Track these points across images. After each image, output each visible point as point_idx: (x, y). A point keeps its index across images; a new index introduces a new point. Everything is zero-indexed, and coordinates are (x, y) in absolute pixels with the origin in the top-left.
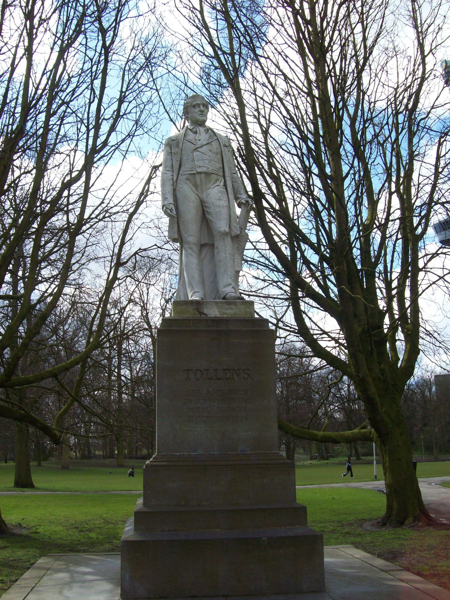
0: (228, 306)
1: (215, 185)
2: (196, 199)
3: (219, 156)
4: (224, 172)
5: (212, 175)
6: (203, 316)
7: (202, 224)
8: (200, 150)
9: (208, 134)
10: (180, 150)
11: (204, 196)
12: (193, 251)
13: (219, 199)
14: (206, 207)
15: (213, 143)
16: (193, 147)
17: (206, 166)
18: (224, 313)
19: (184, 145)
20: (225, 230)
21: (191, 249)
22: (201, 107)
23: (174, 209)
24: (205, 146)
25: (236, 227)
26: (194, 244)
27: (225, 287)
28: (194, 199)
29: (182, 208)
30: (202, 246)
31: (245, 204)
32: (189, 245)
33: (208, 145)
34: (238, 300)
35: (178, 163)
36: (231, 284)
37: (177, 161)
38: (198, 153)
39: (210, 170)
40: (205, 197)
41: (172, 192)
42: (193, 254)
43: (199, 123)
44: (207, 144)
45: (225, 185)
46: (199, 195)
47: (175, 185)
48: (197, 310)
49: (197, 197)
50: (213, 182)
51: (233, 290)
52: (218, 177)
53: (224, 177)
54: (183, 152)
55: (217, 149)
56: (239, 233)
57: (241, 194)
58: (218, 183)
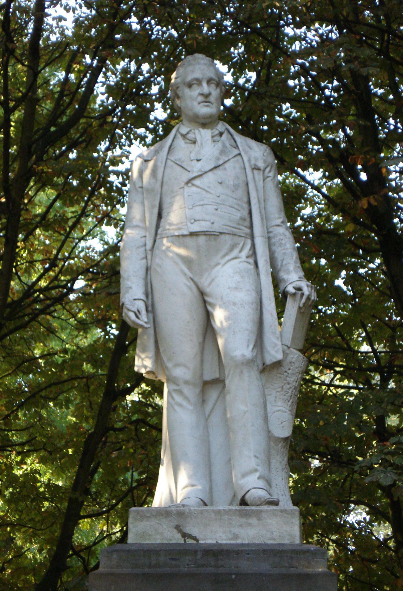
0: (244, 520)
1: (227, 258)
2: (190, 288)
3: (240, 193)
4: (251, 227)
5: (223, 237)
6: (190, 541)
7: (204, 338)
8: (197, 182)
9: (219, 145)
10: (159, 183)
11: (204, 283)
12: (186, 398)
13: (236, 288)
14: (210, 304)
15: (227, 165)
16: (186, 176)
17: (207, 218)
18: (236, 537)
19: (168, 171)
20: (243, 356)
21: (180, 392)
22: (205, 84)
23: (144, 312)
24: (210, 174)
25: (276, 345)
26: (187, 382)
27: (244, 475)
28: (186, 290)
29: (162, 309)
30: (207, 385)
31: (294, 295)
32: (178, 385)
33: (216, 171)
34: (266, 507)
35: (156, 211)
36: (256, 470)
37: (153, 207)
38: (194, 189)
39: (217, 228)
40: (206, 283)
41: (143, 272)
42: (184, 403)
43: (203, 121)
44: (215, 168)
45: (254, 253)
46: (195, 279)
47: (149, 257)
48: (178, 528)
49: (191, 284)
50: (222, 253)
51: (261, 483)
52: (236, 239)
53: (252, 237)
54: (165, 188)
55: (237, 177)
56: (280, 356)
57: (288, 272)
58: (235, 252)
